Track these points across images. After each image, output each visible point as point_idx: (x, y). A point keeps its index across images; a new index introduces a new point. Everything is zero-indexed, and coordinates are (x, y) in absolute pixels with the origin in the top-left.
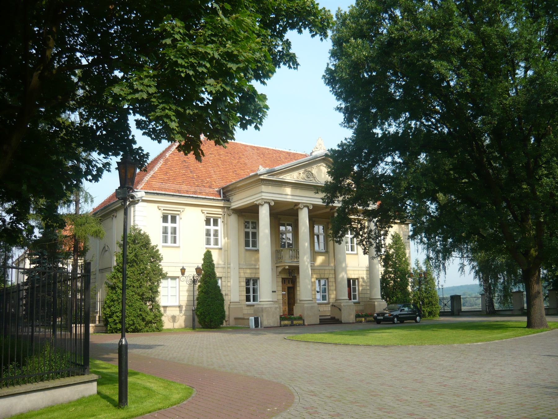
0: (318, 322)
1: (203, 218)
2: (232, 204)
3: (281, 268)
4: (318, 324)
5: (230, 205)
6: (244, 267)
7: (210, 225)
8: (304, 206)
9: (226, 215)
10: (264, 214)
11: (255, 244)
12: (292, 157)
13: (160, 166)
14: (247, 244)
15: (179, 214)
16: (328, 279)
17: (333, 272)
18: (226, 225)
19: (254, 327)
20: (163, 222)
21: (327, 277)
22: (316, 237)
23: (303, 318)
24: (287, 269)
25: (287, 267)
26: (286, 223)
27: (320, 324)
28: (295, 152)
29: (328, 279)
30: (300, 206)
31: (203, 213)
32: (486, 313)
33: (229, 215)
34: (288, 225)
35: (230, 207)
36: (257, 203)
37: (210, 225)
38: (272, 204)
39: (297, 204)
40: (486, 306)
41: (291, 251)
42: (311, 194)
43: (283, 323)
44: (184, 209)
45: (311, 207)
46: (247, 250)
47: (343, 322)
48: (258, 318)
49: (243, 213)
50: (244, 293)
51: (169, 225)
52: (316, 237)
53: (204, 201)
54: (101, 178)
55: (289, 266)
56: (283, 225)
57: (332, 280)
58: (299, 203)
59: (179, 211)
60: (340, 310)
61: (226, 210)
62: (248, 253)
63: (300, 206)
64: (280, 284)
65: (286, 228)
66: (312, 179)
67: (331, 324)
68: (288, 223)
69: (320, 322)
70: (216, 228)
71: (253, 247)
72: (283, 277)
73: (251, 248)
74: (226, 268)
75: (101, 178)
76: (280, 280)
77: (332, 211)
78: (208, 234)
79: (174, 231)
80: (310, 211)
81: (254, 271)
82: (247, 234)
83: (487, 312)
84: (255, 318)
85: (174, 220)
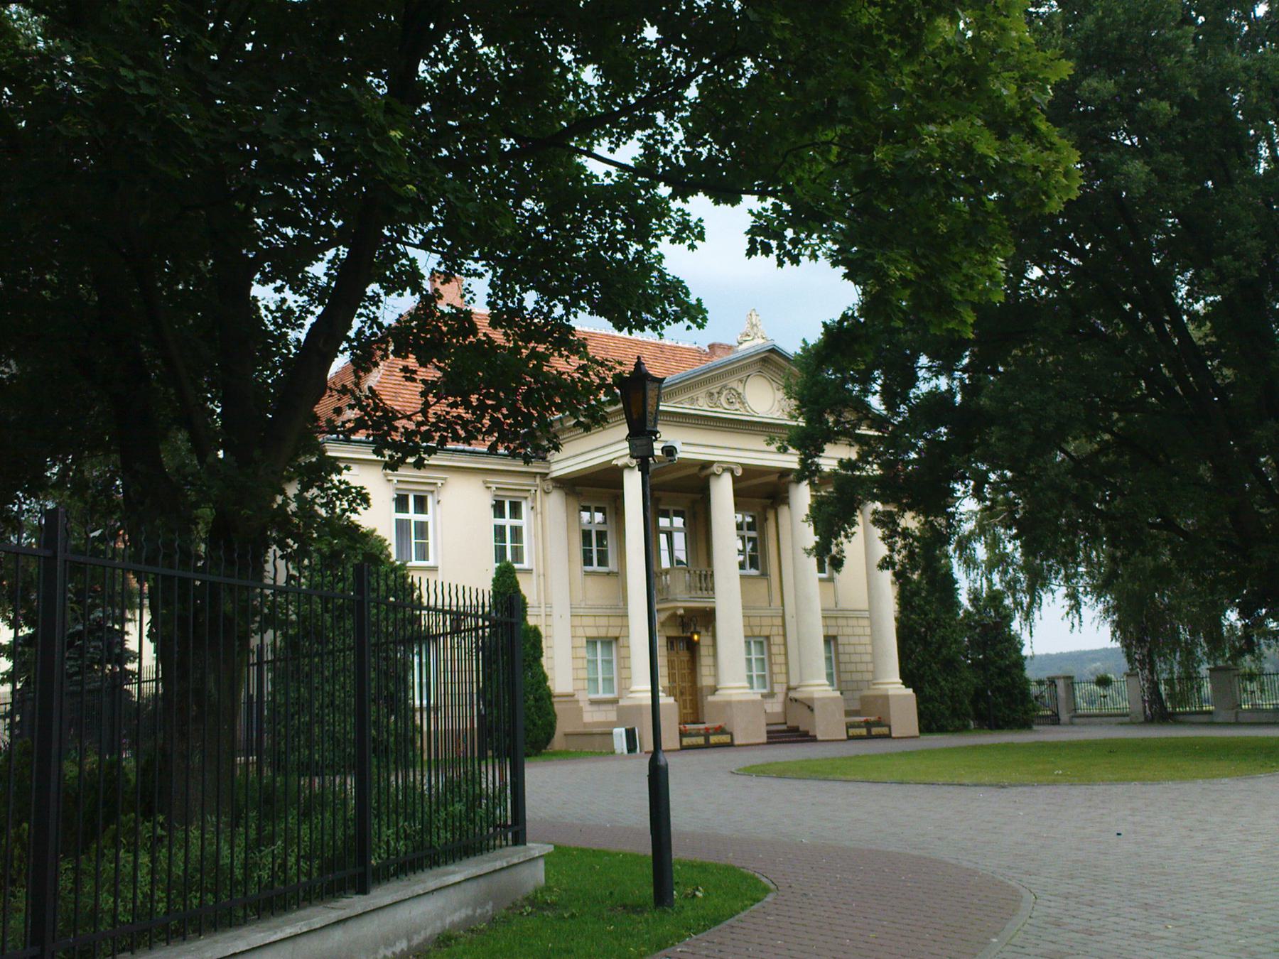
0: (764, 739)
1: (487, 501)
2: (554, 467)
3: (146, 641)
4: (763, 744)
5: (549, 468)
6: (581, 612)
7: (503, 517)
8: (725, 470)
9: (538, 492)
10: (723, 493)
12: (669, 355)
13: (378, 379)
14: (587, 561)
15: (432, 492)
16: (768, 638)
17: (778, 621)
18: (539, 516)
19: (625, 751)
20: (397, 511)
21: (767, 633)
22: (663, 538)
23: (728, 728)
24: (681, 616)
25: (681, 612)
26: (671, 508)
27: (768, 743)
28: (674, 343)
29: (768, 638)
30: (715, 468)
31: (488, 488)
32: (1142, 719)
33: (547, 493)
34: (677, 514)
35: (547, 474)
36: (620, 463)
37: (503, 517)
39: (706, 465)
40: (1144, 701)
41: (687, 575)
42: (758, 443)
43: (686, 741)
44: (445, 479)
45: (739, 473)
46: (587, 573)
47: (819, 737)
48: (633, 730)
49: (578, 489)
50: (583, 674)
51: (508, 522)
52: (663, 538)
53: (473, 458)
54: (846, 276)
55: (685, 609)
56: (666, 514)
57: (777, 640)
58: (711, 463)
59: (435, 484)
60: (811, 709)
61: (538, 480)
62: (589, 580)
63: (715, 468)
65: (671, 522)
66: (737, 406)
67: (783, 742)
68: (676, 508)
69: (768, 738)
70: (516, 522)
71: (599, 565)
72: (669, 635)
73: (595, 567)
74: (543, 615)
75: (846, 276)
77: (784, 480)
78: (500, 531)
79: (422, 529)
80: (736, 480)
81: (618, 621)
83: (1146, 717)
84: (627, 731)
85: (421, 504)
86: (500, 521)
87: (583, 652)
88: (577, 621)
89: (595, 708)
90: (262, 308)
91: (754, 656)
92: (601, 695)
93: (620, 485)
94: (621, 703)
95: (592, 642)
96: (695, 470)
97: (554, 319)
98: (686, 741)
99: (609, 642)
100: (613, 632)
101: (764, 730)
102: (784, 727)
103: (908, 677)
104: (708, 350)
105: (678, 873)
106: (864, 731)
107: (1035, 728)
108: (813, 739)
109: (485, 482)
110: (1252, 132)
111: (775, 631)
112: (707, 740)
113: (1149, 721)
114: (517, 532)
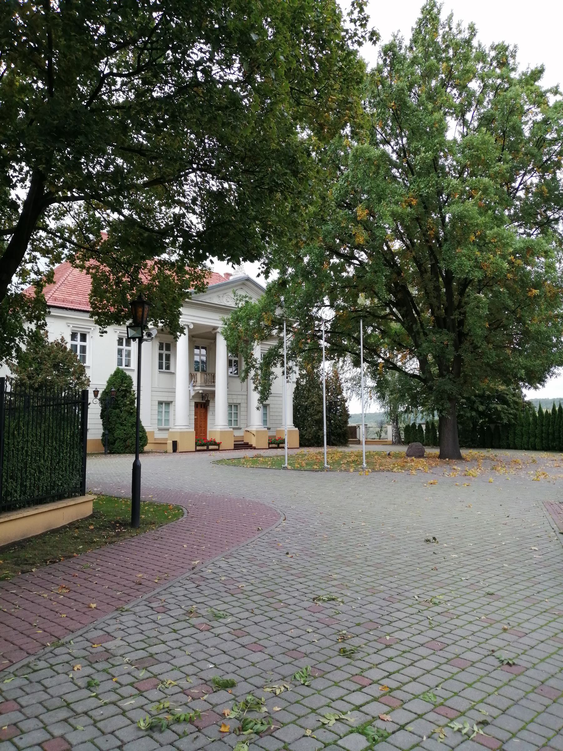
11: (168, 368)
14: (161, 367)
38: (192, 326)
43: (270, 446)
50: (156, 417)
55: (203, 390)
64: (193, 408)
73: (164, 370)
76: (193, 404)
82: (161, 356)
86: (83, 344)
87: (156, 407)
88: (154, 393)
89: (161, 432)
90: (270, 280)
91: (233, 412)
92: (163, 426)
93: (215, 339)
94: (170, 430)
95: (160, 403)
96: (211, 330)
97: (78, 241)
98: (270, 446)
99: (168, 404)
100: (169, 399)
101: (233, 443)
102: (242, 443)
103: (297, 422)
104: (223, 276)
105: (144, 508)
106: (276, 446)
107: (350, 445)
108: (255, 448)
109: (67, 323)
110: (78, 78)
111: (243, 401)
112: (208, 447)
113: (393, 444)
114: (129, 354)
